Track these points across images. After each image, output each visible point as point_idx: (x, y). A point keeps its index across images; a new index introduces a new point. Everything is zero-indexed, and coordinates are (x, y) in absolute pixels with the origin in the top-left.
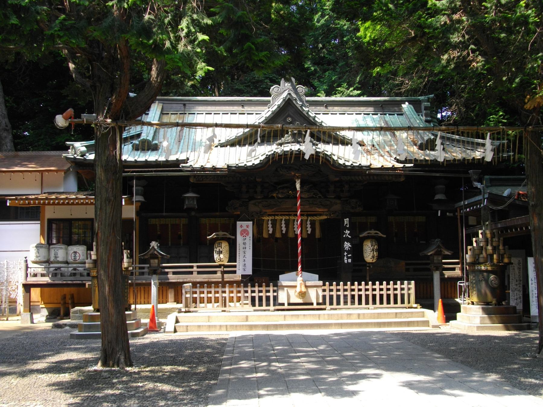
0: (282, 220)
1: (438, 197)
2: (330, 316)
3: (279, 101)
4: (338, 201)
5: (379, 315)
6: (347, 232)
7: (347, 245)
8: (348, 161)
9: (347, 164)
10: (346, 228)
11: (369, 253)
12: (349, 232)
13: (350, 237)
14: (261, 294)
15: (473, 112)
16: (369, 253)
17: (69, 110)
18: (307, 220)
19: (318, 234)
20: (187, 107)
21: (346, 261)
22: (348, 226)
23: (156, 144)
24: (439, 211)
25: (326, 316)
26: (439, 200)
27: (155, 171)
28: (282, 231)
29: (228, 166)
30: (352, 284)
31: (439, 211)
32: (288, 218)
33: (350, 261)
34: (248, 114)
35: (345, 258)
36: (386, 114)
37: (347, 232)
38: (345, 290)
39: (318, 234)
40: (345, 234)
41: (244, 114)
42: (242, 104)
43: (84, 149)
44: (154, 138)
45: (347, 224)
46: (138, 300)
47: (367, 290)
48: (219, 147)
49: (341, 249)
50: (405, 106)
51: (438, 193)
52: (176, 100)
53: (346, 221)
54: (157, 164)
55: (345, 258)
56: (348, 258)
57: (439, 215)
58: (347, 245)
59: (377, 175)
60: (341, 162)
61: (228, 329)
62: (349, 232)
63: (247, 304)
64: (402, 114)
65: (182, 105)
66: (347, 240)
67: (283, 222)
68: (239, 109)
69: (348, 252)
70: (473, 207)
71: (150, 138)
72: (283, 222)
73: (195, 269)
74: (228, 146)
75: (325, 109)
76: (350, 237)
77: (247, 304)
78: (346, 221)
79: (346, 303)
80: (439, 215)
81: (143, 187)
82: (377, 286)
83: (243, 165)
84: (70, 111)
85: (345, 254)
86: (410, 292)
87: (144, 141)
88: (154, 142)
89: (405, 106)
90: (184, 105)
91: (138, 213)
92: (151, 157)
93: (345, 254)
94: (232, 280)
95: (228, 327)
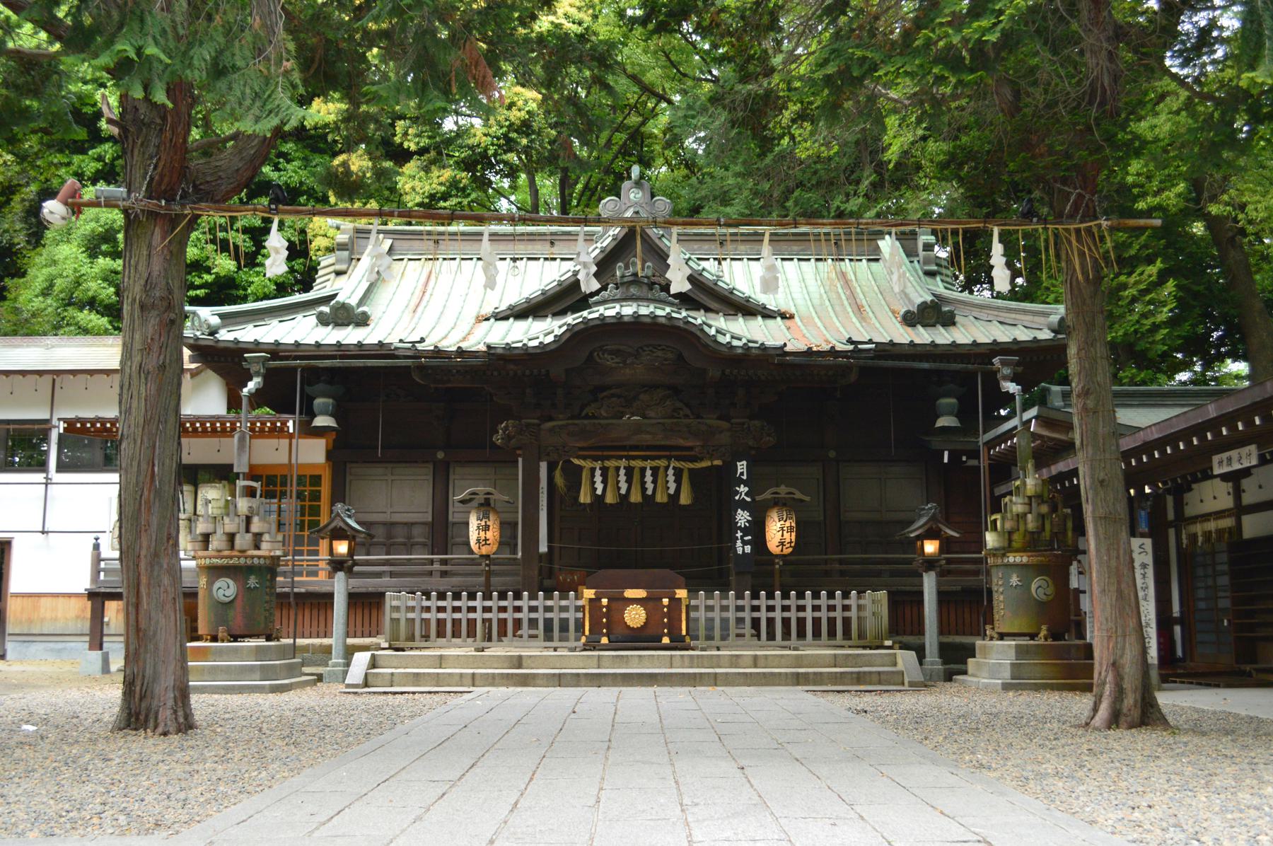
0: (618, 469)
1: (943, 422)
4: (725, 425)
5: (799, 662)
6: (743, 489)
7: (743, 517)
8: (740, 339)
9: (735, 343)
10: (740, 482)
11: (779, 532)
12: (747, 489)
13: (748, 499)
16: (779, 532)
18: (667, 468)
19: (685, 499)
20: (441, 247)
21: (740, 551)
22: (745, 477)
23: (364, 313)
24: (946, 454)
25: (687, 661)
26: (943, 428)
28: (619, 489)
29: (489, 347)
30: (755, 596)
31: (946, 454)
33: (748, 549)
34: (562, 259)
35: (739, 543)
36: (843, 260)
37: (743, 489)
39: (685, 499)
40: (737, 492)
41: (555, 259)
43: (215, 321)
44: (362, 302)
45: (742, 474)
46: (314, 629)
47: (785, 608)
48: (492, 320)
49: (733, 526)
50: (887, 245)
52: (420, 233)
53: (742, 467)
54: (361, 350)
55: (739, 543)
56: (744, 543)
57: (946, 460)
58: (743, 517)
59: (800, 366)
60: (723, 340)
61: (477, 683)
62: (747, 489)
63: (536, 636)
64: (877, 260)
65: (431, 243)
66: (743, 505)
67: (622, 472)
68: (541, 248)
69: (745, 531)
70: (1006, 442)
71: (353, 302)
72: (622, 472)
73: (436, 566)
74: (511, 320)
75: (719, 250)
76: (748, 499)
77: (536, 636)
78: (742, 467)
80: (946, 460)
81: (333, 398)
82: (808, 601)
83: (520, 345)
85: (739, 534)
86: (862, 614)
87: (344, 307)
88: (361, 309)
89: (887, 245)
90: (437, 242)
91: (329, 455)
92: (350, 336)
93: (739, 534)
95: (477, 677)
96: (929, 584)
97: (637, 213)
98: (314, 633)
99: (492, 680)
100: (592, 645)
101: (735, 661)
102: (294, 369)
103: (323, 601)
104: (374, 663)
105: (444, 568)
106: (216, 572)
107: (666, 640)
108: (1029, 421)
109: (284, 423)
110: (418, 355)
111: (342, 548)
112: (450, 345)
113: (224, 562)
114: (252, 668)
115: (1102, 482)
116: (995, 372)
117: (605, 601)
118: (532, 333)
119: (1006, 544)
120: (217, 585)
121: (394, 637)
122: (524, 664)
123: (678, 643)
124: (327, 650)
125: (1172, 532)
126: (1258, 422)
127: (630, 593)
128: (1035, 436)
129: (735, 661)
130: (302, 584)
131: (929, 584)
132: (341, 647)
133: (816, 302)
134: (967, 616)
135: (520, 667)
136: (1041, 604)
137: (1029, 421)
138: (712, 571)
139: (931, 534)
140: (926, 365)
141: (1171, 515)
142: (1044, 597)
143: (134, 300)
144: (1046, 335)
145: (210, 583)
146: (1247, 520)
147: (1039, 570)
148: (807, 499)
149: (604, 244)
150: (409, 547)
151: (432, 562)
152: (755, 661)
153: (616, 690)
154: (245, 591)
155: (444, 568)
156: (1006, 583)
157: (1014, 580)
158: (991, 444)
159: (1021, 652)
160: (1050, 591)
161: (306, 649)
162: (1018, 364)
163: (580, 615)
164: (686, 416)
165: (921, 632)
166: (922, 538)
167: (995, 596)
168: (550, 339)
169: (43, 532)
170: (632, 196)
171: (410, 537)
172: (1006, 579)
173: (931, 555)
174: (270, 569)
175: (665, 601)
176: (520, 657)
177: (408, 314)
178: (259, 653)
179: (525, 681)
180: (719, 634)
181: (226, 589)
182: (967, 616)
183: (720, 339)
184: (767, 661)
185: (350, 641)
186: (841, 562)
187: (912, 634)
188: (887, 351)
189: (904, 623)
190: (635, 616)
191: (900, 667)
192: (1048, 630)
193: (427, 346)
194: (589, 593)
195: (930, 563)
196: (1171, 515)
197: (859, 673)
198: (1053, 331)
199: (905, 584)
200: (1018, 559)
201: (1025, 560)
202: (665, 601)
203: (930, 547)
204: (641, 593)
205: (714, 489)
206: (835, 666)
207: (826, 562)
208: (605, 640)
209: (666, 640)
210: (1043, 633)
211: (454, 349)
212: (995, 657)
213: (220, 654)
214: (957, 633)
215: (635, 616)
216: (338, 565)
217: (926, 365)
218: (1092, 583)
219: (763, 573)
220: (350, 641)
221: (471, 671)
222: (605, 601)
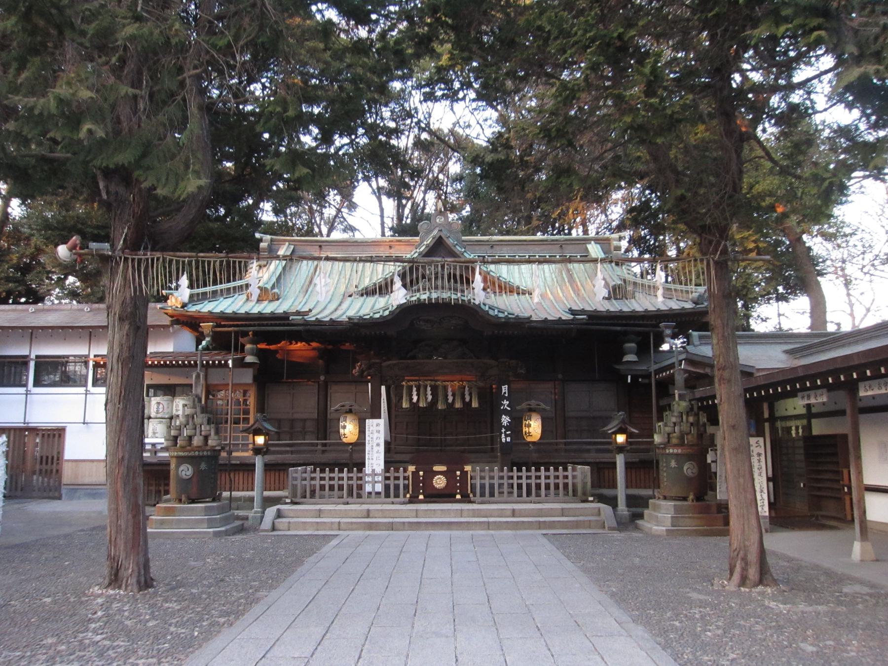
2: (476, 513)
3: (429, 241)
5: (540, 513)
6: (506, 402)
7: (505, 420)
9: (501, 315)
10: (504, 398)
14: (332, 483)
15: (234, 71)
17: (74, 238)
21: (503, 440)
24: (629, 377)
27: (259, 325)
29: (349, 318)
31: (629, 377)
32: (433, 383)
33: (509, 439)
35: (503, 436)
37: (506, 402)
38: (528, 477)
42: (811, 354)
49: (500, 426)
51: (626, 354)
53: (505, 389)
55: (503, 436)
56: (506, 436)
58: (505, 420)
66: (506, 412)
67: (429, 389)
69: (507, 428)
73: (319, 447)
78: (505, 389)
79: (529, 494)
83: (368, 317)
84: (75, 239)
85: (503, 430)
93: (503, 430)
94: (598, 460)
96: (620, 460)
97: (441, 231)
98: (245, 488)
99: (352, 527)
100: (413, 500)
101: (501, 513)
102: (230, 332)
103: (249, 468)
104: (279, 515)
105: (324, 448)
106: (181, 460)
107: (458, 497)
108: (681, 361)
109: (226, 362)
110: (307, 323)
111: (260, 440)
112: (325, 316)
113: (186, 454)
114: (202, 521)
115: (733, 427)
116: (662, 332)
117: (421, 473)
118: (377, 306)
119: (666, 440)
120: (181, 468)
121: (294, 495)
122: (371, 515)
123: (466, 499)
124: (251, 499)
125: (767, 425)
126: (830, 381)
127: (437, 468)
128: (685, 371)
129: (501, 513)
130: (237, 458)
131: (620, 460)
132: (259, 498)
133: (550, 283)
134: (642, 477)
135: (368, 517)
136: (689, 480)
137: (681, 361)
138: (487, 450)
139: (621, 431)
140: (619, 328)
141: (766, 415)
142: (690, 474)
143: (115, 314)
144: (689, 305)
145: (178, 467)
146: (814, 422)
147: (689, 457)
148: (548, 408)
149: (422, 249)
150: (304, 434)
151: (317, 445)
152: (514, 513)
153: (427, 533)
154: (197, 472)
155: (324, 448)
156: (668, 466)
157: (673, 464)
158: (658, 372)
159: (677, 509)
160: (695, 471)
161: (239, 499)
162: (675, 327)
163: (406, 482)
164: (471, 358)
165: (614, 486)
166: (616, 433)
167: (661, 464)
168: (387, 313)
169: (84, 423)
170: (438, 220)
171: (304, 428)
172: (668, 463)
173: (622, 443)
174: (215, 454)
175: (458, 473)
176: (368, 511)
177: (301, 295)
178: (207, 511)
179: (371, 527)
180: (490, 493)
181: (186, 471)
182: (642, 477)
183: (491, 312)
184: (522, 514)
185: (267, 493)
186: (566, 444)
187: (609, 488)
188: (595, 317)
189: (603, 474)
190: (440, 482)
191: (603, 517)
192: (695, 495)
193: (311, 318)
194: (412, 468)
195: (621, 449)
196: (766, 415)
197: (577, 521)
198: (694, 303)
199: (605, 458)
200: (675, 451)
201: (680, 451)
202: (458, 473)
203: (621, 439)
204: (443, 468)
205: (491, 400)
206: (563, 516)
207: (557, 444)
208: (421, 497)
209: (458, 497)
210: (691, 497)
211: (327, 319)
212: (661, 516)
213: (182, 512)
214: (637, 487)
215: (440, 482)
216: (258, 451)
217: (619, 328)
218: (723, 463)
219: (519, 456)
220: (267, 493)
221: (337, 520)
222: (421, 473)
